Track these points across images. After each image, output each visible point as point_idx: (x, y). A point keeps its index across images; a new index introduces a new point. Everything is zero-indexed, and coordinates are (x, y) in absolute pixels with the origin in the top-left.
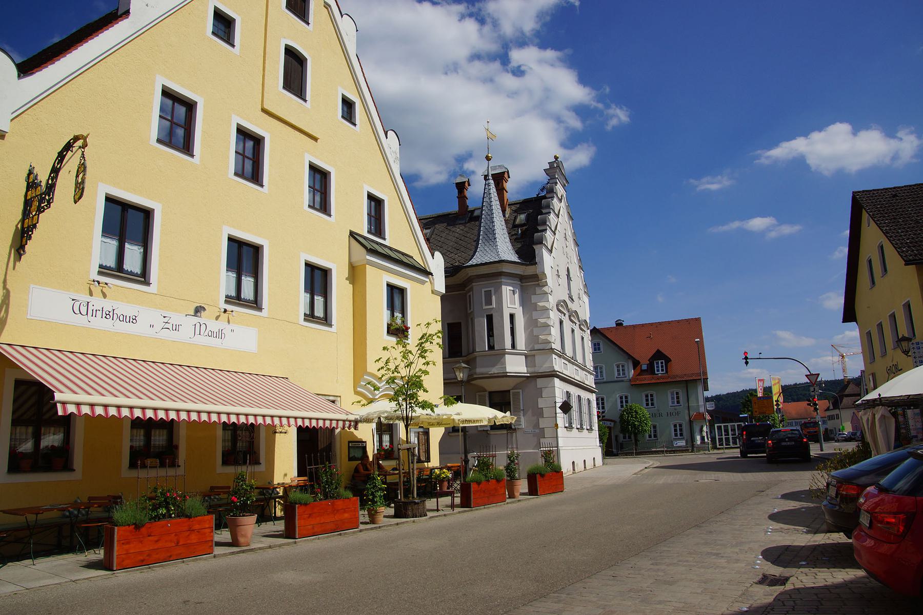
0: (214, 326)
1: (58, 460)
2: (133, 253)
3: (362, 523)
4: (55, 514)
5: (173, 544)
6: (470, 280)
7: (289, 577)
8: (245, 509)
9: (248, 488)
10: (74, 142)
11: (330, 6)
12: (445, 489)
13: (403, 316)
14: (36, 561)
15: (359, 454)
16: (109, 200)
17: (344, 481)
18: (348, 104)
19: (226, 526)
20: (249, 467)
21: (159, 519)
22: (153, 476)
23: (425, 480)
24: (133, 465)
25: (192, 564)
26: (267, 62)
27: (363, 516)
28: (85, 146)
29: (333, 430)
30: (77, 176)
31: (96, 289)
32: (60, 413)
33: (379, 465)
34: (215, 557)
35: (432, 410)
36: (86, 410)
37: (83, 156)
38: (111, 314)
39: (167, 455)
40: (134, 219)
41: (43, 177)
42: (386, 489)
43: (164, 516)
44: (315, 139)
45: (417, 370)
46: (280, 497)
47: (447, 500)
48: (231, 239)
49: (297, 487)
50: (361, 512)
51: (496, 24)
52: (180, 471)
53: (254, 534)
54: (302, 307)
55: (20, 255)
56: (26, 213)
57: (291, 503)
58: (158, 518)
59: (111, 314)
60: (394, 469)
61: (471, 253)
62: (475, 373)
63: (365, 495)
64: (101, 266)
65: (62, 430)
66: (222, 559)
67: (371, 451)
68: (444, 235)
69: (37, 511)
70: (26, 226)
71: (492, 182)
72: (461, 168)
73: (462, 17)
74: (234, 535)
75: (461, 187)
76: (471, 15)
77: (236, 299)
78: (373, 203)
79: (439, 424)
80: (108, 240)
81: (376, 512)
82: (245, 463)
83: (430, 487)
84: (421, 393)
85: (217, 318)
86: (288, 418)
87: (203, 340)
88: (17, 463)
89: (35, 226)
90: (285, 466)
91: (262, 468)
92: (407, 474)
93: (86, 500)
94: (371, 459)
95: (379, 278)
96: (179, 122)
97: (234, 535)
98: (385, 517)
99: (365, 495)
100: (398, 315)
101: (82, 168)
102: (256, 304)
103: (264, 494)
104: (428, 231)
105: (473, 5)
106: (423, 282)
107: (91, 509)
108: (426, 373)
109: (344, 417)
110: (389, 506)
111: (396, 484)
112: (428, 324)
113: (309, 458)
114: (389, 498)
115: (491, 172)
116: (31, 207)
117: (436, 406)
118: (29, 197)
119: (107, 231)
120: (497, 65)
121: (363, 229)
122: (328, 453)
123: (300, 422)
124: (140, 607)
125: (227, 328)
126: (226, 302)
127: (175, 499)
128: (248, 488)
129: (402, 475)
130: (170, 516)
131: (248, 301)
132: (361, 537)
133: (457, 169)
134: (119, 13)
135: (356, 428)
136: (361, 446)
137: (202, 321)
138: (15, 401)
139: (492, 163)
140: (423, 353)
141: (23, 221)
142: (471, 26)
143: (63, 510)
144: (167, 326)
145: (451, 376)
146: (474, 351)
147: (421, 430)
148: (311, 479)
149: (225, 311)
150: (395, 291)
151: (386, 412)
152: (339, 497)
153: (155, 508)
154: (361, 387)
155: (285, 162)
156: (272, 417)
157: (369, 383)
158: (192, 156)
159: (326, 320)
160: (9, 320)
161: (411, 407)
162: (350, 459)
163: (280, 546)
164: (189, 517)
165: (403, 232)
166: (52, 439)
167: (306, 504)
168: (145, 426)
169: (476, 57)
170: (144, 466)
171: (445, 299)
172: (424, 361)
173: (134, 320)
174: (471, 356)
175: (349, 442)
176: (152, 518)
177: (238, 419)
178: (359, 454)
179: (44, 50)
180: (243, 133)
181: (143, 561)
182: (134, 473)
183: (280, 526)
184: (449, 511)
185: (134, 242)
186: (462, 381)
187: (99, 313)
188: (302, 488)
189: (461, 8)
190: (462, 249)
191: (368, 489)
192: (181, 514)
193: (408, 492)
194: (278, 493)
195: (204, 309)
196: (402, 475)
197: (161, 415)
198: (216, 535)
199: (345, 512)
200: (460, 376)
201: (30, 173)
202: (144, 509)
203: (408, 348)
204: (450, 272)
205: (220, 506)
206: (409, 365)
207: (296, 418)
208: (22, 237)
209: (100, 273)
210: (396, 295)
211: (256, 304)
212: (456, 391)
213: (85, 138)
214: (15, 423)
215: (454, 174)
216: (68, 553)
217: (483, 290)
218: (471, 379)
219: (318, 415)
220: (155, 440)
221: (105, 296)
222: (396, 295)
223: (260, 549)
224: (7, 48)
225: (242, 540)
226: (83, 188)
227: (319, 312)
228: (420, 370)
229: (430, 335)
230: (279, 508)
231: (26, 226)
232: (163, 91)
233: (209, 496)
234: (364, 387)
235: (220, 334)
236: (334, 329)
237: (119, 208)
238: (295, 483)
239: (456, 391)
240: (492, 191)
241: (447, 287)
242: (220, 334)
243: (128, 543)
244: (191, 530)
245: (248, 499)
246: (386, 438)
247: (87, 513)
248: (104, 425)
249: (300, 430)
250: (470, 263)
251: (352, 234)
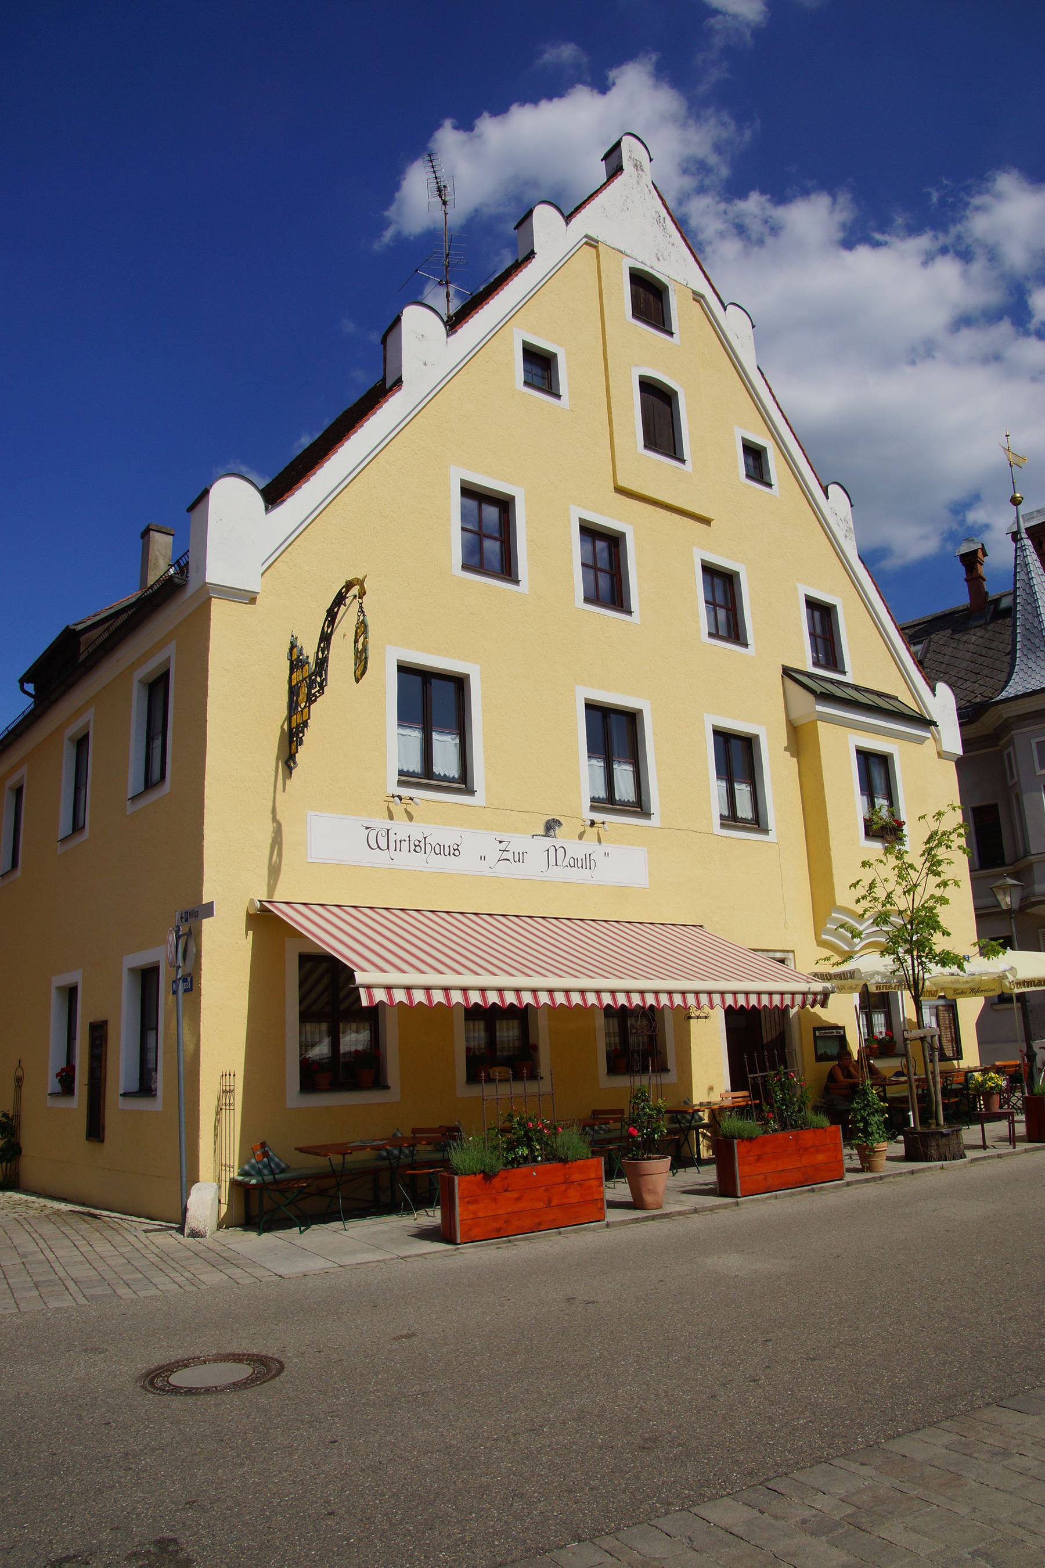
0: (577, 849)
1: (362, 1072)
2: (445, 745)
3: (849, 1170)
4: (368, 1154)
5: (542, 1205)
6: (1007, 726)
7: (730, 1263)
8: (651, 1148)
9: (654, 1113)
10: (347, 591)
11: (703, 297)
12: (996, 1109)
13: (891, 804)
14: (349, 1224)
15: (833, 1049)
16: (405, 670)
17: (812, 1097)
18: (754, 454)
19: (621, 1175)
20: (653, 1079)
21: (519, 1164)
22: (502, 1093)
23: (956, 1093)
24: (472, 1078)
25: (573, 1236)
26: (613, 410)
27: (850, 1157)
28: (362, 594)
29: (784, 1011)
30: (356, 641)
31: (398, 808)
32: (365, 1003)
33: (871, 1068)
34: (608, 1225)
35: (960, 966)
36: (400, 996)
37: (361, 610)
38: (422, 844)
39: (522, 1062)
40: (442, 693)
41: (310, 649)
42: (888, 1110)
43: (525, 1159)
44: (707, 522)
45: (926, 896)
46: (704, 1126)
47: (1000, 1128)
48: (591, 707)
49: (732, 1109)
50: (847, 1151)
51: (993, 256)
52: (545, 1086)
53: (667, 1188)
54: (717, 806)
55: (290, 769)
56: (293, 707)
57: (725, 1136)
58: (516, 1162)
59: (422, 844)
60: (899, 1074)
61: (1003, 676)
62: (1034, 894)
63: (851, 1122)
64: (401, 773)
65: (367, 1025)
66: (616, 1232)
67: (854, 1042)
68: (948, 651)
69: (344, 1150)
70: (294, 725)
71: (1027, 542)
72: (962, 522)
73: (928, 259)
74: (636, 1190)
75: (971, 561)
76: (944, 251)
77: (607, 801)
78: (817, 614)
79: (974, 991)
80: (407, 731)
81: (872, 1150)
82: (645, 1070)
83: (966, 1104)
84: (937, 937)
85: (581, 836)
86: (710, 993)
87: (562, 873)
88: (313, 1076)
89: (305, 724)
90: (709, 1073)
91: (671, 1078)
92: (923, 1082)
93: (408, 1134)
94: (855, 1057)
95: (841, 741)
96: (491, 534)
97: (636, 1190)
98: (889, 1159)
99: (851, 1122)
100: (881, 802)
101: (362, 628)
102: (639, 807)
103: (679, 1122)
104: (919, 647)
105: (946, 231)
106: (921, 740)
107: (419, 1147)
108: (943, 901)
109: (803, 987)
110: (892, 1138)
111: (904, 1100)
112: (939, 814)
113: (751, 1059)
114: (895, 1126)
115: (1024, 526)
116: (298, 696)
117: (967, 958)
118: (294, 683)
119: (405, 718)
120: (1005, 327)
121: (804, 660)
122: (780, 1045)
123: (729, 1000)
124: (502, 1305)
125: (599, 852)
126: (593, 808)
127: (541, 1131)
128: (654, 1113)
129: (914, 1084)
130: (535, 1160)
131: (627, 804)
132: (847, 1194)
133: (955, 526)
134: (388, 386)
135: (824, 1004)
136: (836, 1035)
137: (558, 842)
138: (301, 984)
139: (1023, 509)
140: (934, 866)
141: (289, 718)
142: (947, 270)
143: (378, 1148)
144: (506, 855)
145: (987, 901)
146: (1027, 853)
147: (942, 1002)
148: (755, 1095)
149: (593, 823)
150: (872, 761)
151: (878, 973)
152: (805, 1125)
153: (511, 1147)
154: (829, 932)
155: (663, 570)
156: (683, 993)
157: (842, 926)
158: (517, 582)
159: (758, 823)
160: (284, 867)
161: (921, 963)
162: (820, 1058)
163: (712, 1209)
164: (564, 1161)
165: (875, 656)
166: (354, 1040)
167: (750, 1139)
168: (484, 1015)
169: (964, 321)
170: (490, 1080)
171: (965, 766)
172: (938, 880)
173: (455, 851)
174: (1022, 864)
175: (815, 1029)
176: (508, 1163)
177: (629, 999)
178: (833, 1049)
179: (292, 463)
180: (589, 532)
181: (499, 1230)
182: (475, 1091)
183: (709, 1175)
184: (1005, 1148)
185: (445, 730)
186: (1009, 911)
187: (405, 845)
188: (741, 1111)
189: (924, 242)
190: (986, 672)
191: (854, 1110)
192: (552, 1156)
193: (926, 1114)
194: (701, 1119)
195: (560, 823)
196: (914, 1084)
197: (510, 998)
198: (607, 1190)
199: (818, 1151)
200: (1006, 901)
201: (293, 646)
202: (495, 1148)
203: (907, 859)
204: (967, 715)
205: (609, 1141)
206: (910, 890)
207: (722, 993)
208: (291, 742)
209: (401, 783)
210: (875, 770)
211: (639, 807)
212: (999, 929)
213: (361, 583)
214: (305, 1017)
215: (951, 537)
216: (390, 1213)
217: (1034, 741)
218: (1026, 904)
219: (760, 986)
220: (502, 1038)
221: (410, 817)
222: (875, 770)
223: (680, 1213)
224: (243, 469)
225: (649, 1198)
226: (366, 658)
227: (745, 810)
228: (932, 897)
229: (944, 834)
230: (704, 1144)
231: (294, 725)
233: (592, 1126)
234: (834, 933)
235: (587, 862)
236: (772, 836)
237: (419, 679)
238: (728, 1103)
239: (999, 929)
240: (1029, 560)
241: (965, 743)
242: (587, 862)
243: (475, 1202)
244: (568, 1182)
245: (654, 1131)
246: (879, 1019)
247: (413, 1155)
248: (426, 1018)
249: (729, 1012)
250: (1004, 694)
251: (788, 672)
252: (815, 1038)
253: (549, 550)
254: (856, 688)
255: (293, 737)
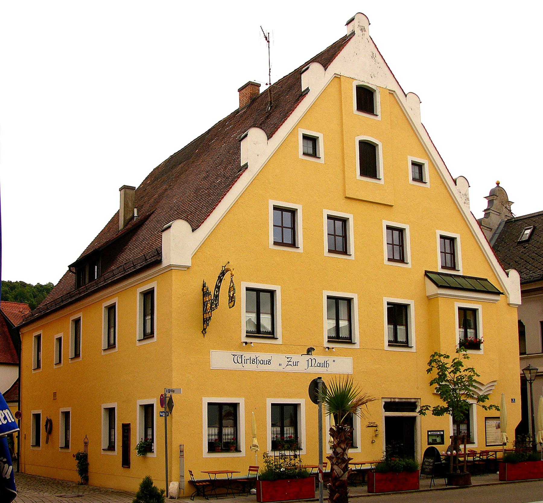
0: (321, 359)
30: (229, 292)
38: (255, 360)
40: (265, 298)
41: (212, 289)
44: (392, 206)
56: (205, 312)
59: (255, 360)
64: (329, 337)
95: (452, 303)
131: (346, 338)
137: (312, 357)
144: (290, 363)
173: (269, 362)
175: (428, 431)
187: (248, 361)
195: (314, 349)
201: (204, 286)
210: (468, 318)
232: (274, 208)
235: (325, 364)
252: (428, 435)
253: (313, 232)
254: (464, 277)
255: (206, 321)
